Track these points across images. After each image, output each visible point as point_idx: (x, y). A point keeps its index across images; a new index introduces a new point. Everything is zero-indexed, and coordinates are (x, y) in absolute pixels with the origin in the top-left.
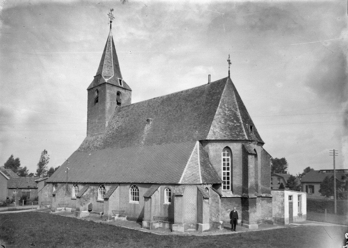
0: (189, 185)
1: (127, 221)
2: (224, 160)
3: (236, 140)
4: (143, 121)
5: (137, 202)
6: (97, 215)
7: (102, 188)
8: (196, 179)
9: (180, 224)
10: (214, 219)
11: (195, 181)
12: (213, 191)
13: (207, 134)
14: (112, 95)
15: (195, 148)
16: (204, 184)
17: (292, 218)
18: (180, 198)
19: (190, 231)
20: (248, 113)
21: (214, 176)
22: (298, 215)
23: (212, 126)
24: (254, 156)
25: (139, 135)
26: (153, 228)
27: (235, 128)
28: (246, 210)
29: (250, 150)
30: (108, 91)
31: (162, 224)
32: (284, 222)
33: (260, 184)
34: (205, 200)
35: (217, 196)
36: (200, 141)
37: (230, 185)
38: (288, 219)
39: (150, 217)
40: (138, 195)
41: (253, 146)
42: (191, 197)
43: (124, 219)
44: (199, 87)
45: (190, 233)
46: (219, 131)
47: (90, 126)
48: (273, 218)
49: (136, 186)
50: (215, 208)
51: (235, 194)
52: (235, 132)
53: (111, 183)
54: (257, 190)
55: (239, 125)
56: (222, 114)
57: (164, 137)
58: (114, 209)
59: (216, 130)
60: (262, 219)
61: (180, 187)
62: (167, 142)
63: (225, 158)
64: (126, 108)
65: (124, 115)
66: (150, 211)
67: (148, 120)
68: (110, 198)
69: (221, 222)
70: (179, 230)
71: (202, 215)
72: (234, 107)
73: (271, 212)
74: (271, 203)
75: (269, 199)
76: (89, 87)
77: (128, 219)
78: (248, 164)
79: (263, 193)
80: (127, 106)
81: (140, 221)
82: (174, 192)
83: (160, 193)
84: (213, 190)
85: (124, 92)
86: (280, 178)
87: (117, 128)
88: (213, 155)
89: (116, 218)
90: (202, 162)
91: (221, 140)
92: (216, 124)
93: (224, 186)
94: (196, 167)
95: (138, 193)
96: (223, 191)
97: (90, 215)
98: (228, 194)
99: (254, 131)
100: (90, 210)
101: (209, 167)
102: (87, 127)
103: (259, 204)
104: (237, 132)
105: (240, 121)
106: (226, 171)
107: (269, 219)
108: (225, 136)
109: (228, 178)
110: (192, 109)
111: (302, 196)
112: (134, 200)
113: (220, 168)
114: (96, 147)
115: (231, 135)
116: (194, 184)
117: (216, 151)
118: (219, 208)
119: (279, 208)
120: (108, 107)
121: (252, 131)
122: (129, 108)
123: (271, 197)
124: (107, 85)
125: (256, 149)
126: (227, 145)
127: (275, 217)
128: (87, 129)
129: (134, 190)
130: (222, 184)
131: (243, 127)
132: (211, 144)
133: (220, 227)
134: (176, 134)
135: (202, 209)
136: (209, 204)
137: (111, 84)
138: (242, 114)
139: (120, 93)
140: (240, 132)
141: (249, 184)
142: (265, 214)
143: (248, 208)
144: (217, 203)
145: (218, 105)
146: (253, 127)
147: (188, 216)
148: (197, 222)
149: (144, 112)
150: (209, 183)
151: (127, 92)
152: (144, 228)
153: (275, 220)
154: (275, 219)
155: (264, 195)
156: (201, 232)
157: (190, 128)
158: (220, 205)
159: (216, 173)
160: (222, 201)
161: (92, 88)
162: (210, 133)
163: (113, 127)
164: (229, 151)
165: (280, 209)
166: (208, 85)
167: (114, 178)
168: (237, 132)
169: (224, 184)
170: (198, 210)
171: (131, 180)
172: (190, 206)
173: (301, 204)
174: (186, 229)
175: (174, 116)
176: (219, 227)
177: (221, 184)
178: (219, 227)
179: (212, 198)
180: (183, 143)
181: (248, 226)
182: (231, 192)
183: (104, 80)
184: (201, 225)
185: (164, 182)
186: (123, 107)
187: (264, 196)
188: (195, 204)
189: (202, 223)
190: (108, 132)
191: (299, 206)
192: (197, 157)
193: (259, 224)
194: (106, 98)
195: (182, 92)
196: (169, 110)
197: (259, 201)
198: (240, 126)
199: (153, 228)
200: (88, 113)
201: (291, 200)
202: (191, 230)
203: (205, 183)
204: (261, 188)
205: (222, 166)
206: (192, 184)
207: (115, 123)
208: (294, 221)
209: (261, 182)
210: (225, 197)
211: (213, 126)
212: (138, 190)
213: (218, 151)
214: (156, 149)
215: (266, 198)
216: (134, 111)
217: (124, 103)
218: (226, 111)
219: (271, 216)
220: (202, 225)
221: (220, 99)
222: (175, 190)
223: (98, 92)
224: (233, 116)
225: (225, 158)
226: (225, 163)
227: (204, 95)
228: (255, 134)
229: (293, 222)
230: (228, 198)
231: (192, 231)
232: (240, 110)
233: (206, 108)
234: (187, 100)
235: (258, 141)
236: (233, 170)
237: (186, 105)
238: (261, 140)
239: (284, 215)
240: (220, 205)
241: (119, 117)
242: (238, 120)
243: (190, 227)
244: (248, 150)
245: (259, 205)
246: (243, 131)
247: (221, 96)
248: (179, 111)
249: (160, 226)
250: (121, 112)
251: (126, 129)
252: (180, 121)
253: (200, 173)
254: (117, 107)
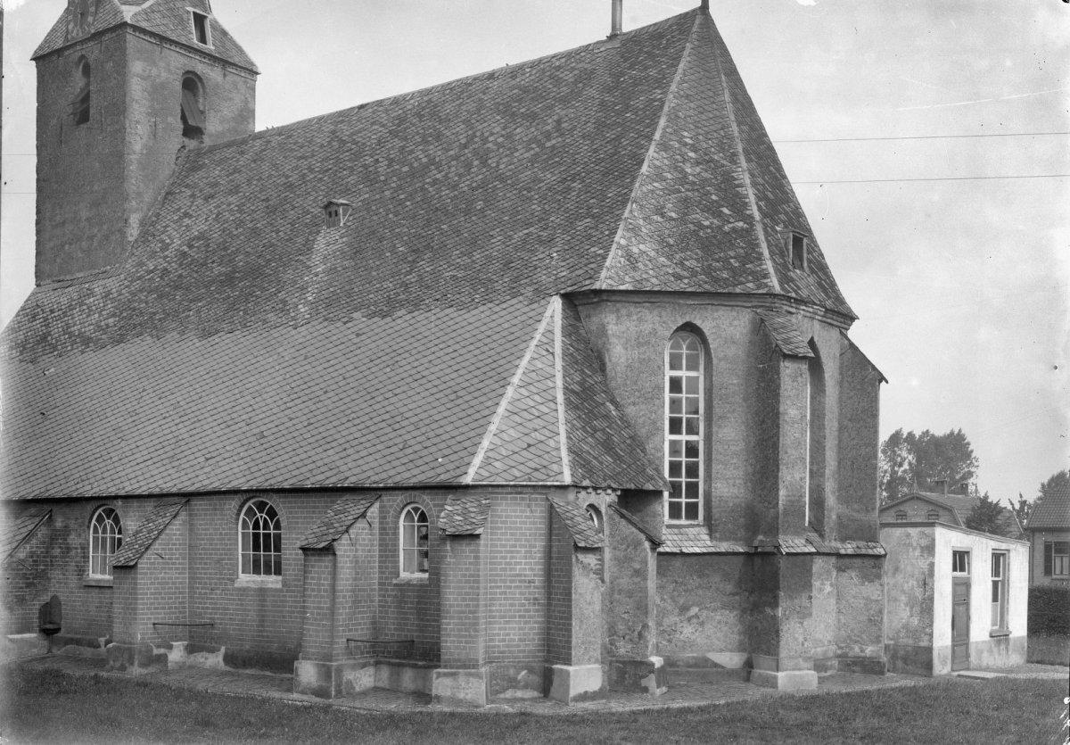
0: (509, 490)
1: (228, 669)
2: (675, 385)
3: (729, 294)
4: (308, 212)
5: (273, 578)
6: (82, 648)
7: (108, 522)
8: (545, 463)
9: (469, 665)
10: (623, 649)
11: (536, 474)
12: (624, 522)
13: (601, 267)
14: (157, 90)
15: (542, 327)
16: (577, 487)
17: (964, 648)
18: (465, 548)
19: (515, 700)
20: (784, 177)
21: (627, 458)
22: (991, 636)
23: (621, 227)
24: (804, 367)
25: (289, 275)
26: (346, 691)
27: (728, 239)
28: (768, 610)
29: (787, 341)
30: (136, 67)
31: (385, 672)
32: (929, 666)
33: (831, 500)
34: (581, 557)
35: (638, 544)
36: (570, 299)
37: (701, 501)
38: (949, 652)
39: (332, 643)
40: (278, 549)
41: (802, 328)
42: (521, 546)
43: (215, 660)
44: (569, 55)
45: (512, 707)
46: (653, 254)
47: (50, 240)
48: (887, 647)
49: (268, 504)
50: (630, 597)
51: (721, 540)
52: (726, 260)
53: (150, 496)
54: (817, 526)
55: (742, 229)
56: (669, 176)
57: (406, 286)
58: (161, 616)
59: (642, 247)
60: (839, 652)
61: (470, 503)
62: (417, 306)
63: (681, 378)
64: (228, 153)
65: (216, 184)
66: (333, 614)
67: (330, 203)
68: (143, 564)
69: (657, 661)
70: (461, 696)
71: (570, 625)
72: (721, 147)
73: (875, 621)
74: (877, 583)
75: (871, 564)
76: (40, 48)
77: (229, 659)
78: (778, 402)
79: (843, 540)
80: (229, 145)
81: (279, 663)
82: (442, 522)
83: (377, 531)
84: (622, 516)
85: (220, 79)
86: (941, 512)
87: (185, 248)
88: (622, 360)
89: (176, 655)
90: (573, 391)
91: (659, 292)
92: (641, 222)
93: (671, 504)
94: (546, 410)
95: (278, 538)
96: (669, 527)
97: (50, 651)
98: (694, 539)
99: (810, 261)
100: (48, 626)
101: (607, 417)
102: (38, 243)
103: (828, 589)
104: (732, 261)
105: (748, 212)
106: (684, 438)
107: (869, 650)
108: (678, 277)
109: (692, 471)
110: (537, 154)
111: (1012, 554)
112: (256, 571)
113: (654, 423)
114: (80, 335)
115: (708, 271)
116: (534, 486)
117: (641, 342)
118: (647, 598)
119: (911, 603)
120: (138, 147)
121: (801, 260)
122: (242, 153)
123: (878, 557)
124: (131, 39)
125: (816, 339)
126: (687, 319)
127: (892, 642)
128: (38, 254)
129: (256, 526)
130: (666, 494)
131: (762, 236)
132: (618, 310)
133: (651, 682)
134: (458, 267)
135: (570, 600)
136: (603, 581)
137: (152, 34)
138: (760, 180)
139: (200, 79)
140: (745, 260)
141: (782, 493)
142: (852, 630)
143: (776, 598)
144: (640, 573)
145: (653, 134)
146: (805, 241)
147: (508, 635)
148: (546, 661)
149: (311, 170)
150: (604, 485)
151: (233, 77)
152: (303, 693)
153: (894, 657)
154: (893, 652)
155: (849, 548)
156: (563, 701)
157: (524, 241)
158: (652, 583)
159: (636, 443)
160: (661, 572)
161: (59, 52)
162: (614, 258)
163: (163, 241)
164: (697, 339)
165: (917, 609)
166: (609, 46)
167: (165, 474)
168: (732, 261)
169: (671, 495)
170: (549, 604)
171: (243, 480)
172: (516, 587)
173: (1006, 592)
174: (498, 692)
175: (455, 187)
176: (644, 682)
177: (658, 494)
178: (644, 682)
179: (617, 553)
180: (490, 305)
181: (775, 678)
182: (704, 530)
183: (117, 12)
184: (562, 670)
185: (398, 479)
186: (212, 149)
187: (850, 551)
188: (539, 581)
189: (568, 661)
190: (141, 264)
191: (995, 599)
192: (553, 366)
193: (823, 674)
194: (128, 99)
195: (491, 76)
196: (432, 162)
197: (828, 572)
198: (749, 231)
199: (344, 693)
200: (38, 174)
201: (962, 569)
202: (519, 694)
203: (586, 483)
204: (839, 517)
205: (667, 414)
206: (523, 486)
207: (175, 222)
208: (973, 659)
209: (839, 491)
210: (676, 550)
211: (628, 230)
212: (277, 526)
213: (648, 343)
214: (363, 337)
215: (858, 561)
216: (265, 166)
217: (220, 128)
218: (688, 165)
219: (878, 640)
220: (570, 669)
221: (662, 107)
222: (449, 514)
223: (87, 71)
224: (719, 188)
225: (681, 378)
226: (680, 400)
227: (592, 92)
228: (813, 271)
229: (972, 666)
230: (694, 559)
231: (523, 700)
232: (749, 160)
233: (596, 151)
234: (513, 114)
235: (829, 304)
236: (715, 429)
237: (509, 137)
238: (840, 300)
239: (931, 635)
240: (652, 583)
241: (193, 196)
242: (739, 207)
243: (513, 683)
244: (778, 338)
245: (826, 591)
246: (760, 257)
247: (665, 93)
248: (476, 163)
249: (380, 684)
250: (201, 173)
251: (225, 249)
252: (479, 207)
253: (563, 438)
254: (183, 147)
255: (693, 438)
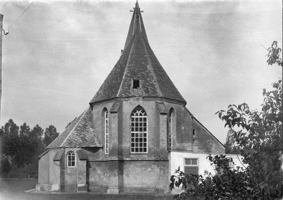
0: (52, 149)
255: (145, 132)
